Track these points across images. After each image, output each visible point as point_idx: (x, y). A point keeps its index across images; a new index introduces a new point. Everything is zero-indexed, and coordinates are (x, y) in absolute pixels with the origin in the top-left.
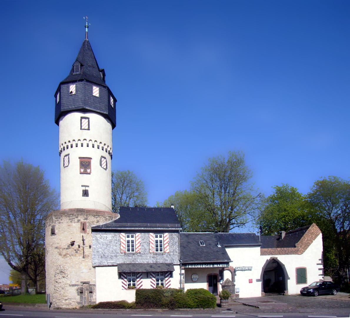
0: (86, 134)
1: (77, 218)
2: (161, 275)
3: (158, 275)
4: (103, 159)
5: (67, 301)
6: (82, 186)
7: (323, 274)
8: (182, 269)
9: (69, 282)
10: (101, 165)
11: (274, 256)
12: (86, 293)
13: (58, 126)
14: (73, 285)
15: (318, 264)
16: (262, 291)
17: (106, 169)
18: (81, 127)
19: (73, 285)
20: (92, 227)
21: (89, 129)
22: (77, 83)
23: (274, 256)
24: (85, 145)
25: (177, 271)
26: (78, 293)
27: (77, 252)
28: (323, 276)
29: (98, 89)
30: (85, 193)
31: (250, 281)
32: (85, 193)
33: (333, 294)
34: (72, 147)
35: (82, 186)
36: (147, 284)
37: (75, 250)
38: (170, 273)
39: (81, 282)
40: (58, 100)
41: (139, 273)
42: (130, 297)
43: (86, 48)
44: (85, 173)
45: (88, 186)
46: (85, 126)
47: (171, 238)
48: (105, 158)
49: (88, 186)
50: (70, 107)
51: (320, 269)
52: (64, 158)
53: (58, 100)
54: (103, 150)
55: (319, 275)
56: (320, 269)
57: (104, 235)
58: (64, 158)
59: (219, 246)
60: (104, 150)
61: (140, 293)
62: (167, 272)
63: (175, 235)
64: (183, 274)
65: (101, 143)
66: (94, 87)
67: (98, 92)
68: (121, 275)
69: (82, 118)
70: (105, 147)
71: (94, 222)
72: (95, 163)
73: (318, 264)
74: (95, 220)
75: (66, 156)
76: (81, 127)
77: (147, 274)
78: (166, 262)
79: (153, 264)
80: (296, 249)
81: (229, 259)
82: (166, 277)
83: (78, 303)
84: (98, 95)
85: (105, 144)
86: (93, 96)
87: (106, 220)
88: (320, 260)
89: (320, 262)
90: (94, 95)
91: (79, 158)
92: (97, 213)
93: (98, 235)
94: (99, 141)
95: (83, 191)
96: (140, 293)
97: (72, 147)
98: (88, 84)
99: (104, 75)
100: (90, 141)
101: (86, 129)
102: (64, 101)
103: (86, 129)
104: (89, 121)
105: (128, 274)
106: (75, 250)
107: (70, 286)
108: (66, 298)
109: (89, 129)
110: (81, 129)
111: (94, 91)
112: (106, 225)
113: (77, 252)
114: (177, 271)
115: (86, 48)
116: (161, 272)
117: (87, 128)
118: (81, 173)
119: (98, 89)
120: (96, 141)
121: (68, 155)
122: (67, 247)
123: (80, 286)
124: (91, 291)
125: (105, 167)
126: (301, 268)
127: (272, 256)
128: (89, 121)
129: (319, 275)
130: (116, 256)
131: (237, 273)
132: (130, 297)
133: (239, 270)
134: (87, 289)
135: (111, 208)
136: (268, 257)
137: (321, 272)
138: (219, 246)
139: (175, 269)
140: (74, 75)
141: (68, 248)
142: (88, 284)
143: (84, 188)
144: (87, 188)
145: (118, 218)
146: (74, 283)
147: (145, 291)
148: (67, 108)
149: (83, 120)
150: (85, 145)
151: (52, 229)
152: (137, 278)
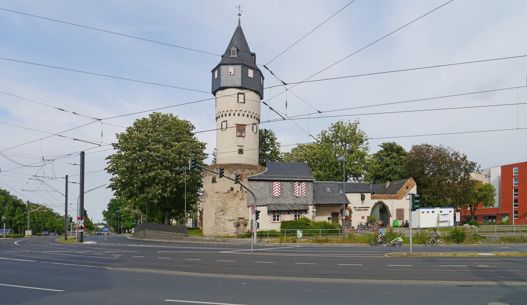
0: (243, 107)
9: (227, 218)
10: (253, 130)
12: (242, 226)
14: (231, 220)
17: (256, 133)
18: (238, 100)
19: (231, 220)
21: (244, 103)
23: (382, 200)
25: (311, 208)
30: (241, 152)
31: (253, 57)
32: (241, 152)
33: (151, 115)
38: (306, 211)
40: (216, 77)
42: (277, 227)
44: (241, 136)
46: (241, 100)
47: (307, 186)
53: (216, 77)
57: (257, 183)
61: (284, 224)
63: (310, 184)
64: (314, 212)
66: (249, 70)
69: (239, 94)
70: (254, 115)
72: (248, 129)
76: (238, 100)
77: (289, 212)
80: (397, 195)
84: (252, 77)
86: (240, 64)
87: (258, 172)
93: (252, 183)
94: (252, 112)
96: (284, 224)
99: (255, 58)
102: (223, 78)
104: (244, 96)
105: (275, 213)
109: (244, 103)
112: (258, 176)
114: (311, 208)
117: (243, 101)
121: (226, 121)
128: (244, 96)
130: (265, 199)
132: (277, 227)
134: (242, 223)
135: (257, 161)
136: (376, 201)
138: (341, 192)
140: (232, 58)
141: (228, 192)
143: (240, 148)
144: (242, 148)
146: (232, 218)
147: (397, 176)
149: (240, 95)
150: (241, 115)
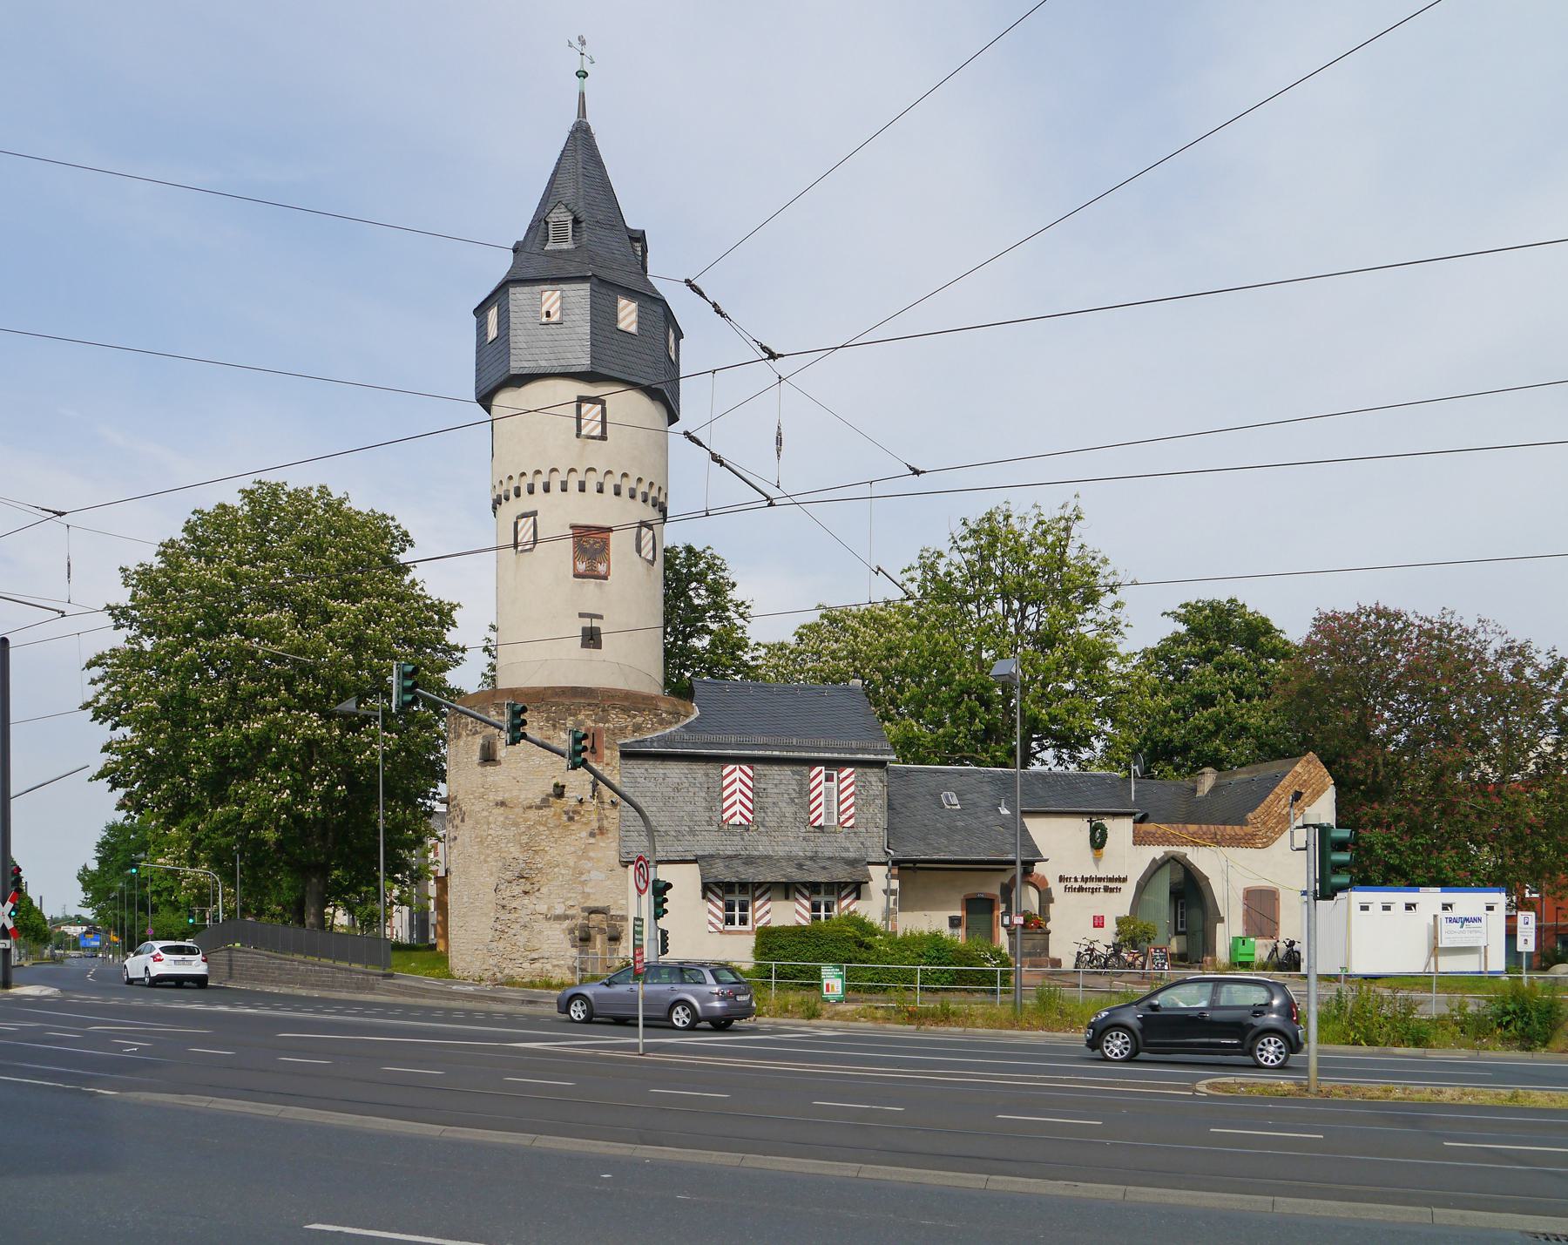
0: (599, 456)
1: (575, 715)
2: (827, 893)
3: (818, 893)
4: (644, 530)
5: (537, 965)
6: (581, 615)
8: (893, 877)
9: (542, 908)
10: (639, 550)
11: (1175, 848)
12: (599, 942)
14: (558, 918)
17: (652, 562)
19: (558, 918)
20: (623, 745)
21: (603, 437)
24: (591, 487)
25: (879, 877)
26: (573, 941)
27: (571, 819)
29: (634, 306)
30: (591, 638)
32: (591, 638)
34: (531, 492)
35: (581, 615)
36: (789, 914)
37: (566, 813)
38: (857, 888)
39: (584, 910)
40: (492, 332)
41: (760, 884)
43: (1097, 860)
45: (601, 617)
48: (650, 527)
49: (601, 617)
50: (543, 363)
52: (516, 524)
53: (492, 332)
54: (633, 497)
58: (516, 524)
59: (1005, 811)
60: (639, 497)
62: (847, 884)
63: (873, 775)
64: (893, 892)
65: (625, 475)
66: (622, 302)
67: (634, 317)
68: (708, 889)
69: (582, 400)
70: (644, 487)
71: (621, 728)
72: (620, 544)
74: (629, 722)
75: (524, 516)
77: (787, 890)
78: (844, 855)
79: (806, 858)
81: (1039, 853)
82: (846, 897)
83: (573, 970)
84: (633, 329)
85: (651, 484)
87: (662, 722)
90: (621, 326)
91: (572, 527)
92: (630, 702)
93: (639, 769)
95: (584, 629)
96: (768, 940)
97: (531, 492)
98: (603, 291)
99: (645, 251)
100: (591, 474)
101: (593, 438)
103: (593, 438)
104: (604, 411)
106: (566, 813)
107: (547, 919)
108: (535, 955)
110: (578, 435)
111: (621, 315)
113: (571, 819)
114: (879, 877)
115: (1097, 860)
116: (827, 884)
117: (597, 432)
118: (577, 575)
119: (634, 306)
120: (625, 475)
122: (538, 801)
123: (580, 921)
124: (614, 934)
125: (650, 557)
128: (604, 411)
130: (692, 832)
134: (602, 931)
136: (1157, 852)
138: (1005, 811)
141: (545, 803)
142: (601, 916)
143: (587, 622)
144: (596, 623)
145: (692, 718)
146: (559, 910)
148: (532, 364)
149: (586, 407)
151: (483, 746)
152: (755, 899)
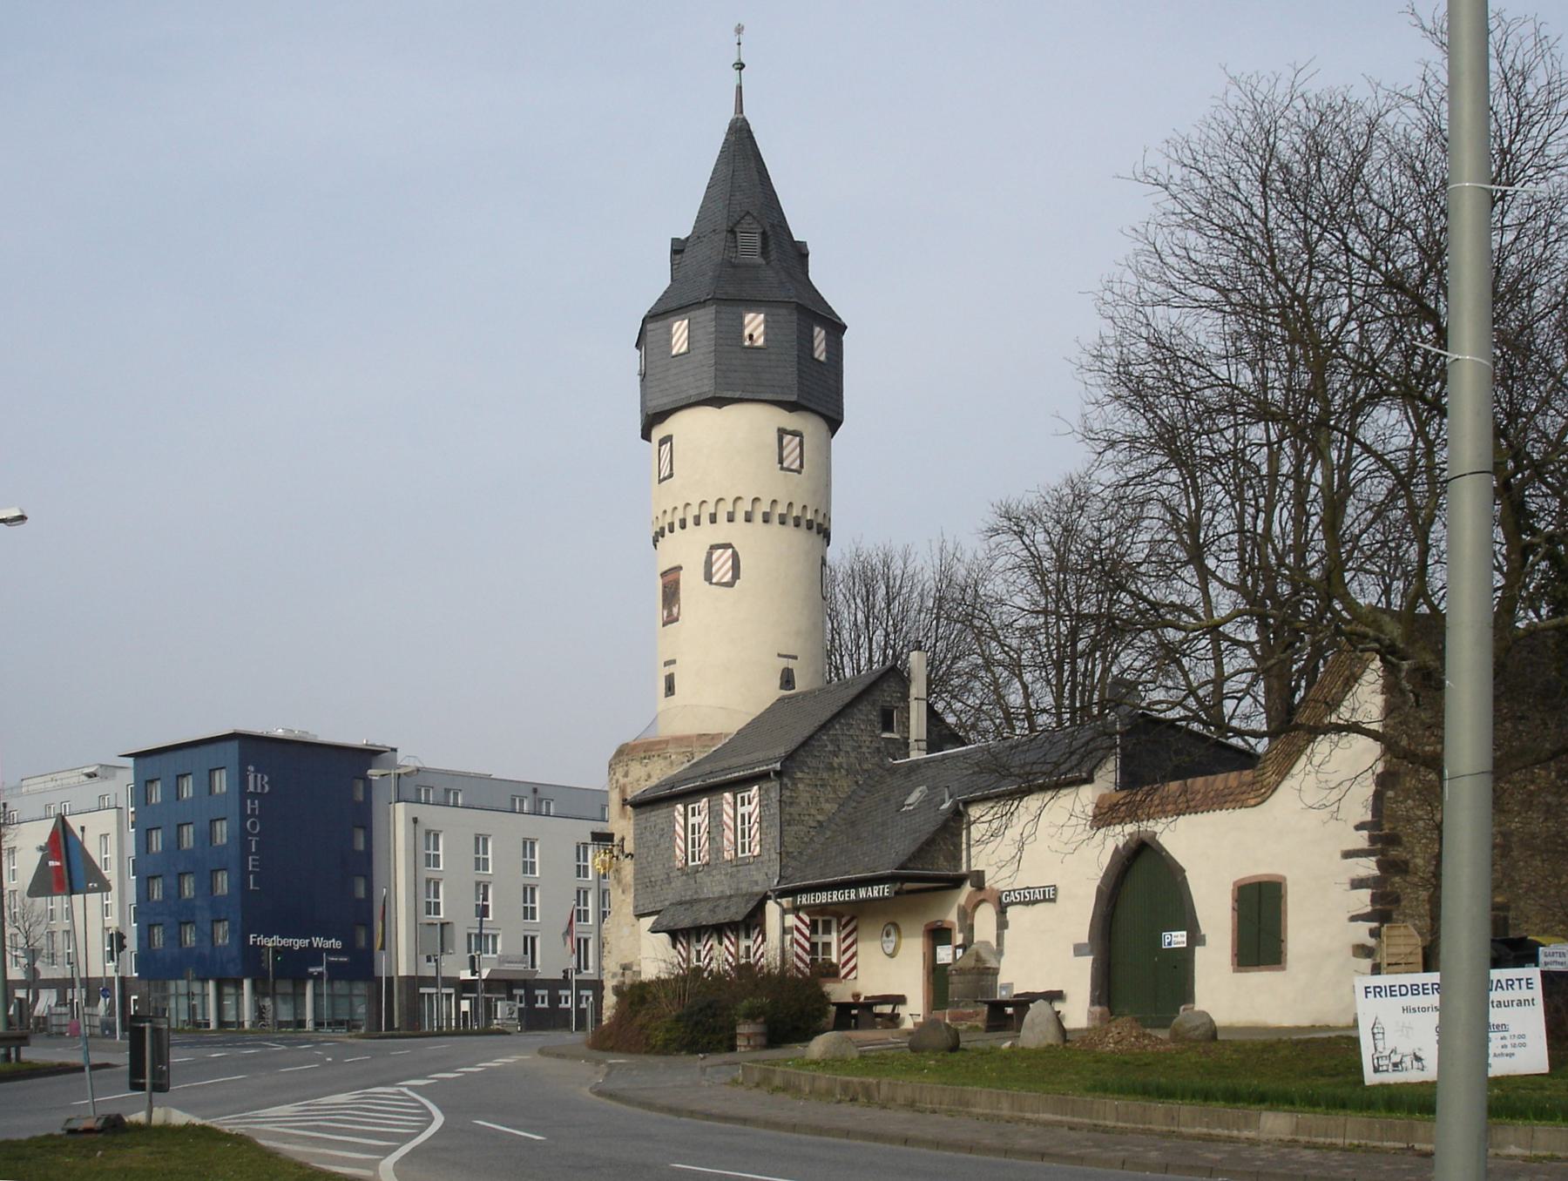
7: (1374, 911)
13: (741, 146)
15: (1348, 855)
16: (1093, 1003)
22: (692, 314)
28: (1375, 925)
48: (795, 433)
51: (1357, 884)
55: (1354, 919)
56: (1357, 884)
73: (1348, 855)
88: (1358, 827)
89: (1361, 840)
97: (683, 526)
112: (671, 783)
126: (1260, 884)
127: (1130, 828)
129: (1354, 919)
131: (1011, 912)
133: (1012, 903)
137: (1362, 900)
139: (1056, 988)
